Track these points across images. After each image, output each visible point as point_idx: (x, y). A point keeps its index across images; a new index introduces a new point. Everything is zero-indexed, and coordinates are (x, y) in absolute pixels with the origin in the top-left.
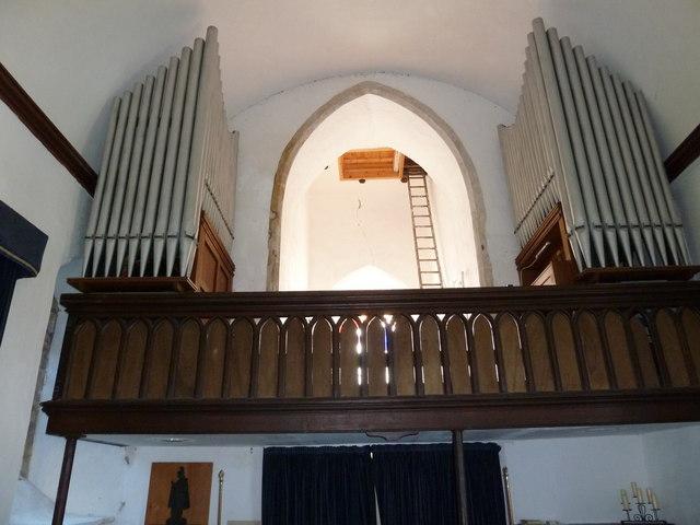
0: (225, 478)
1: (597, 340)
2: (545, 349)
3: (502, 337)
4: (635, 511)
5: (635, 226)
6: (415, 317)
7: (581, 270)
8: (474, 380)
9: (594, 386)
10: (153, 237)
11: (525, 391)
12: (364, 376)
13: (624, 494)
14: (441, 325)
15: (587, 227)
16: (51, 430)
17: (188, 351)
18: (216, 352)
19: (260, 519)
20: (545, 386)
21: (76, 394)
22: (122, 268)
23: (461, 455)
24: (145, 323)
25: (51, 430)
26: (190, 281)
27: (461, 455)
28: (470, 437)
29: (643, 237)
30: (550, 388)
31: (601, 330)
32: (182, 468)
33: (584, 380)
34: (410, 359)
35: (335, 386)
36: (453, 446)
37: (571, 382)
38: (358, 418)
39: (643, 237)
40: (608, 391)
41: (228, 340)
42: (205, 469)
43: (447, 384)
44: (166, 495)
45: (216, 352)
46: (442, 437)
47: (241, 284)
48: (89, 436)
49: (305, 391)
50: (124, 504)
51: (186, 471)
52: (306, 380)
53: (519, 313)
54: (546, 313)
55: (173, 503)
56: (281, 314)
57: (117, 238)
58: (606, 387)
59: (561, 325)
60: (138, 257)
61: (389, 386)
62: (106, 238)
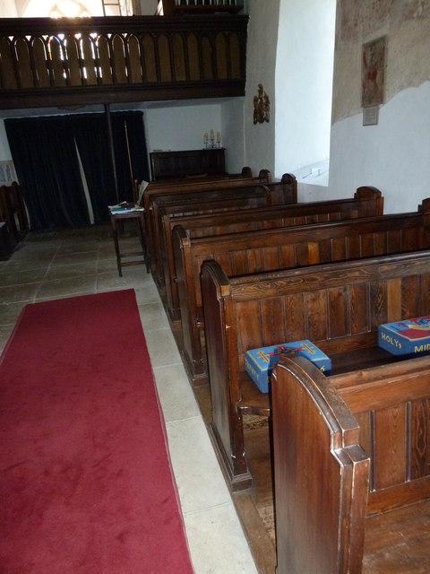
9: (178, 79)
11: (141, 82)
12: (82, 73)
13: (206, 136)
19: (11, 159)
20: (152, 79)
23: (109, 117)
24: (151, 35)
27: (109, 117)
28: (115, 108)
30: (155, 80)
35: (35, 82)
43: (144, 77)
46: (99, 110)
52: (17, 78)
53: (139, 34)
58: (184, 79)
59: (163, 40)
61: (128, 78)
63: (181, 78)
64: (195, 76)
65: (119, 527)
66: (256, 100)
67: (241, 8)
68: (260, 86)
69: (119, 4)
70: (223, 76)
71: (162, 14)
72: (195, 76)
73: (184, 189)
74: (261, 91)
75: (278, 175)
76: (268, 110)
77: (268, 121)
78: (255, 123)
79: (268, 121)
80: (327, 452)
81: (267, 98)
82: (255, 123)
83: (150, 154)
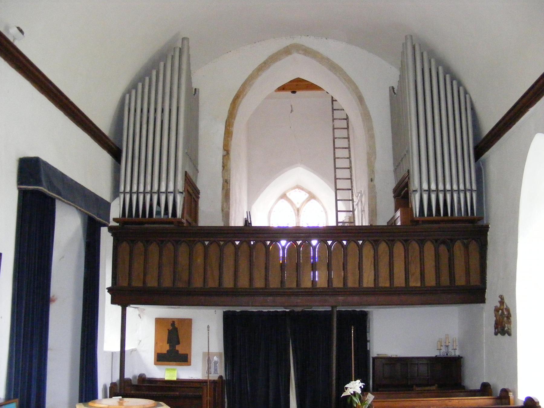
0: (210, 329)
1: (418, 260)
2: (388, 263)
3: (364, 255)
4: (444, 350)
5: (469, 190)
6: (345, 242)
7: (414, 217)
8: (345, 279)
9: (287, 285)
10: (151, 193)
14: (329, 247)
15: (173, 193)
16: (113, 302)
17: (183, 260)
18: (200, 260)
20: (384, 283)
21: (124, 283)
22: (136, 209)
25: (113, 302)
26: (400, 216)
29: (151, 200)
31: (422, 252)
32: (175, 320)
33: (251, 280)
34: (309, 267)
36: (505, 314)
37: (399, 281)
38: (279, 299)
39: (151, 200)
40: (419, 287)
41: (236, 254)
42: (188, 323)
44: (165, 337)
45: (200, 260)
47: (204, 221)
48: (131, 305)
49: (235, 284)
50: (140, 341)
51: (176, 323)
54: (406, 241)
55: (170, 341)
56: (236, 239)
57: (145, 193)
59: (399, 249)
60: (159, 204)
62: (131, 193)
63: (415, 283)
64: (431, 281)
65: (450, 296)
66: (497, 310)
67: (481, 219)
68: (501, 297)
69: (352, 200)
70: (460, 281)
71: (399, 223)
72: (431, 281)
73: (248, 387)
74: (502, 302)
75: (521, 397)
76: (509, 323)
77: (510, 334)
78: (496, 334)
79: (510, 334)
80: (340, 228)
81: (508, 310)
82: (496, 334)
83: (374, 359)
